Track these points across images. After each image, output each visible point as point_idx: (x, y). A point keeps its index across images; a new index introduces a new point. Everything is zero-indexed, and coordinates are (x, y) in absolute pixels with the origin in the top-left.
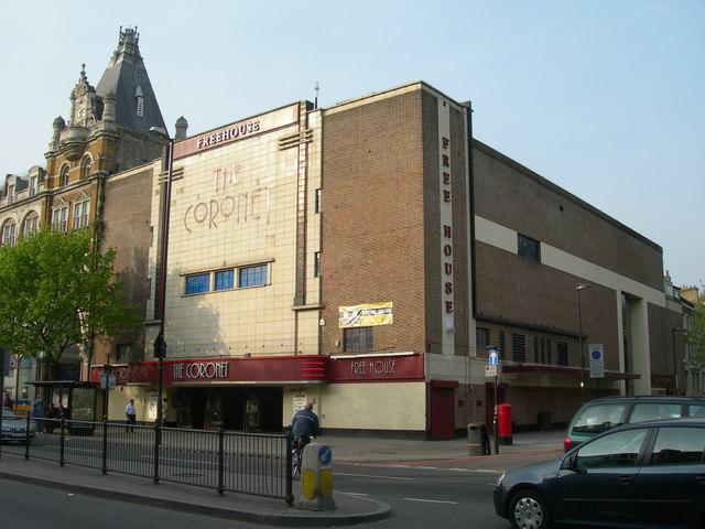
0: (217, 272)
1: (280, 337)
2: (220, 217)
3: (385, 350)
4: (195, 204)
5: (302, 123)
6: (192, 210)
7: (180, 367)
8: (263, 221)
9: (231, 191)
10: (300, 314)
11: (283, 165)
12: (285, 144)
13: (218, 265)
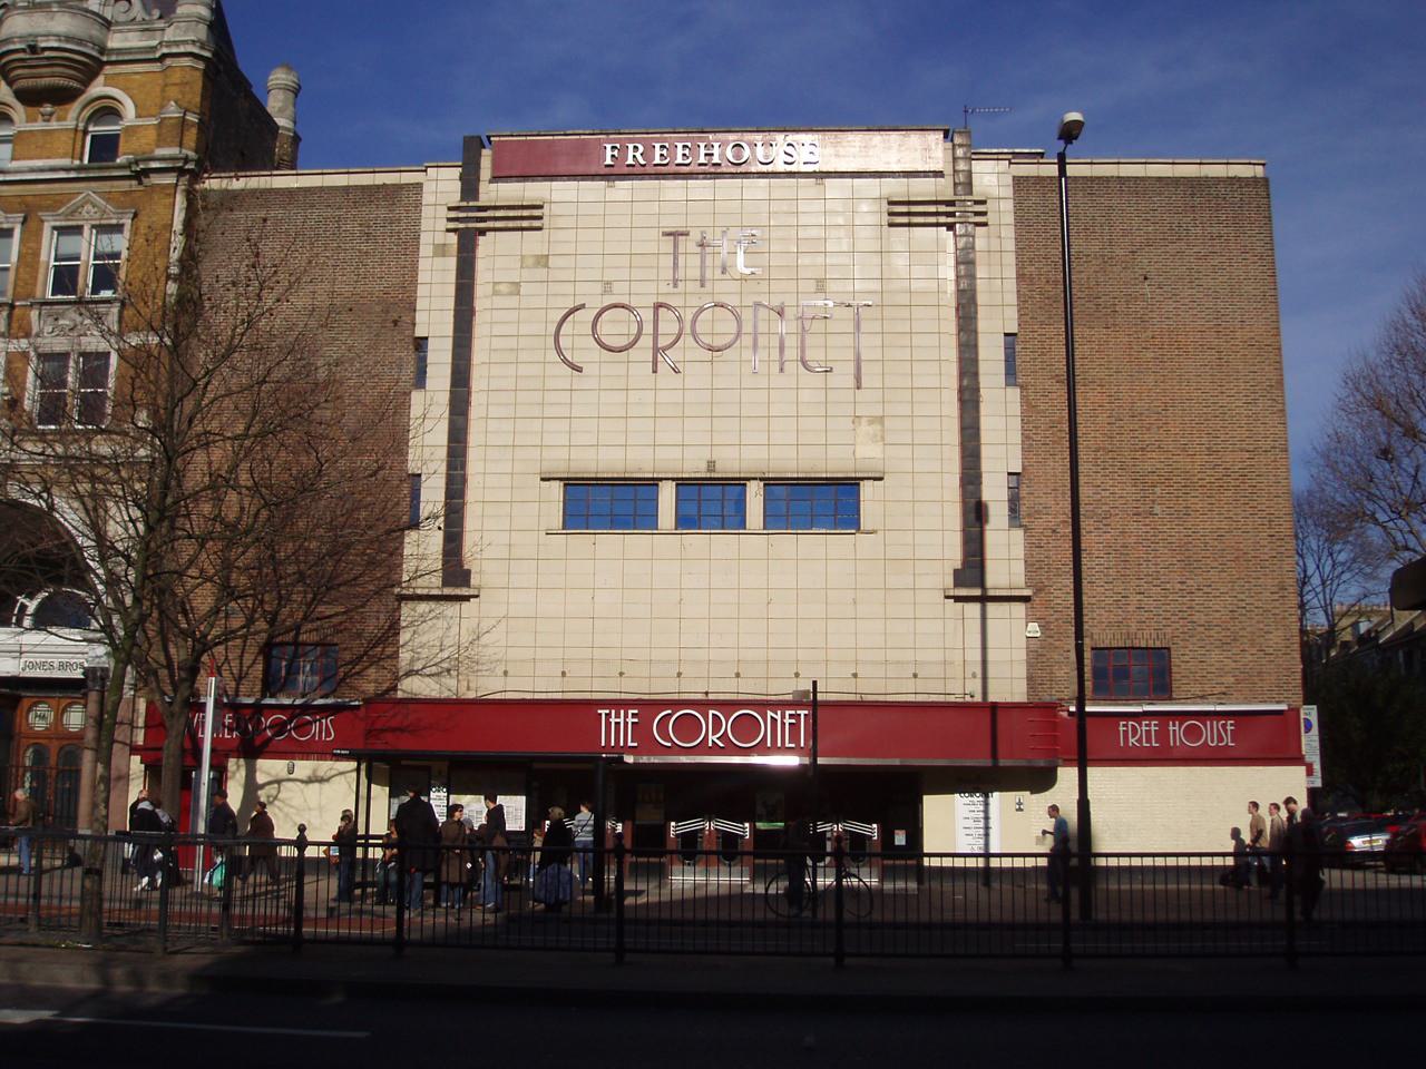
0: (682, 483)
1: (909, 655)
2: (687, 351)
3: (1203, 698)
4: (596, 303)
5: (950, 220)
6: (586, 316)
7: (1310, 588)
8: (843, 376)
9: (726, 291)
11: (900, 262)
12: (903, 213)
13: (695, 466)
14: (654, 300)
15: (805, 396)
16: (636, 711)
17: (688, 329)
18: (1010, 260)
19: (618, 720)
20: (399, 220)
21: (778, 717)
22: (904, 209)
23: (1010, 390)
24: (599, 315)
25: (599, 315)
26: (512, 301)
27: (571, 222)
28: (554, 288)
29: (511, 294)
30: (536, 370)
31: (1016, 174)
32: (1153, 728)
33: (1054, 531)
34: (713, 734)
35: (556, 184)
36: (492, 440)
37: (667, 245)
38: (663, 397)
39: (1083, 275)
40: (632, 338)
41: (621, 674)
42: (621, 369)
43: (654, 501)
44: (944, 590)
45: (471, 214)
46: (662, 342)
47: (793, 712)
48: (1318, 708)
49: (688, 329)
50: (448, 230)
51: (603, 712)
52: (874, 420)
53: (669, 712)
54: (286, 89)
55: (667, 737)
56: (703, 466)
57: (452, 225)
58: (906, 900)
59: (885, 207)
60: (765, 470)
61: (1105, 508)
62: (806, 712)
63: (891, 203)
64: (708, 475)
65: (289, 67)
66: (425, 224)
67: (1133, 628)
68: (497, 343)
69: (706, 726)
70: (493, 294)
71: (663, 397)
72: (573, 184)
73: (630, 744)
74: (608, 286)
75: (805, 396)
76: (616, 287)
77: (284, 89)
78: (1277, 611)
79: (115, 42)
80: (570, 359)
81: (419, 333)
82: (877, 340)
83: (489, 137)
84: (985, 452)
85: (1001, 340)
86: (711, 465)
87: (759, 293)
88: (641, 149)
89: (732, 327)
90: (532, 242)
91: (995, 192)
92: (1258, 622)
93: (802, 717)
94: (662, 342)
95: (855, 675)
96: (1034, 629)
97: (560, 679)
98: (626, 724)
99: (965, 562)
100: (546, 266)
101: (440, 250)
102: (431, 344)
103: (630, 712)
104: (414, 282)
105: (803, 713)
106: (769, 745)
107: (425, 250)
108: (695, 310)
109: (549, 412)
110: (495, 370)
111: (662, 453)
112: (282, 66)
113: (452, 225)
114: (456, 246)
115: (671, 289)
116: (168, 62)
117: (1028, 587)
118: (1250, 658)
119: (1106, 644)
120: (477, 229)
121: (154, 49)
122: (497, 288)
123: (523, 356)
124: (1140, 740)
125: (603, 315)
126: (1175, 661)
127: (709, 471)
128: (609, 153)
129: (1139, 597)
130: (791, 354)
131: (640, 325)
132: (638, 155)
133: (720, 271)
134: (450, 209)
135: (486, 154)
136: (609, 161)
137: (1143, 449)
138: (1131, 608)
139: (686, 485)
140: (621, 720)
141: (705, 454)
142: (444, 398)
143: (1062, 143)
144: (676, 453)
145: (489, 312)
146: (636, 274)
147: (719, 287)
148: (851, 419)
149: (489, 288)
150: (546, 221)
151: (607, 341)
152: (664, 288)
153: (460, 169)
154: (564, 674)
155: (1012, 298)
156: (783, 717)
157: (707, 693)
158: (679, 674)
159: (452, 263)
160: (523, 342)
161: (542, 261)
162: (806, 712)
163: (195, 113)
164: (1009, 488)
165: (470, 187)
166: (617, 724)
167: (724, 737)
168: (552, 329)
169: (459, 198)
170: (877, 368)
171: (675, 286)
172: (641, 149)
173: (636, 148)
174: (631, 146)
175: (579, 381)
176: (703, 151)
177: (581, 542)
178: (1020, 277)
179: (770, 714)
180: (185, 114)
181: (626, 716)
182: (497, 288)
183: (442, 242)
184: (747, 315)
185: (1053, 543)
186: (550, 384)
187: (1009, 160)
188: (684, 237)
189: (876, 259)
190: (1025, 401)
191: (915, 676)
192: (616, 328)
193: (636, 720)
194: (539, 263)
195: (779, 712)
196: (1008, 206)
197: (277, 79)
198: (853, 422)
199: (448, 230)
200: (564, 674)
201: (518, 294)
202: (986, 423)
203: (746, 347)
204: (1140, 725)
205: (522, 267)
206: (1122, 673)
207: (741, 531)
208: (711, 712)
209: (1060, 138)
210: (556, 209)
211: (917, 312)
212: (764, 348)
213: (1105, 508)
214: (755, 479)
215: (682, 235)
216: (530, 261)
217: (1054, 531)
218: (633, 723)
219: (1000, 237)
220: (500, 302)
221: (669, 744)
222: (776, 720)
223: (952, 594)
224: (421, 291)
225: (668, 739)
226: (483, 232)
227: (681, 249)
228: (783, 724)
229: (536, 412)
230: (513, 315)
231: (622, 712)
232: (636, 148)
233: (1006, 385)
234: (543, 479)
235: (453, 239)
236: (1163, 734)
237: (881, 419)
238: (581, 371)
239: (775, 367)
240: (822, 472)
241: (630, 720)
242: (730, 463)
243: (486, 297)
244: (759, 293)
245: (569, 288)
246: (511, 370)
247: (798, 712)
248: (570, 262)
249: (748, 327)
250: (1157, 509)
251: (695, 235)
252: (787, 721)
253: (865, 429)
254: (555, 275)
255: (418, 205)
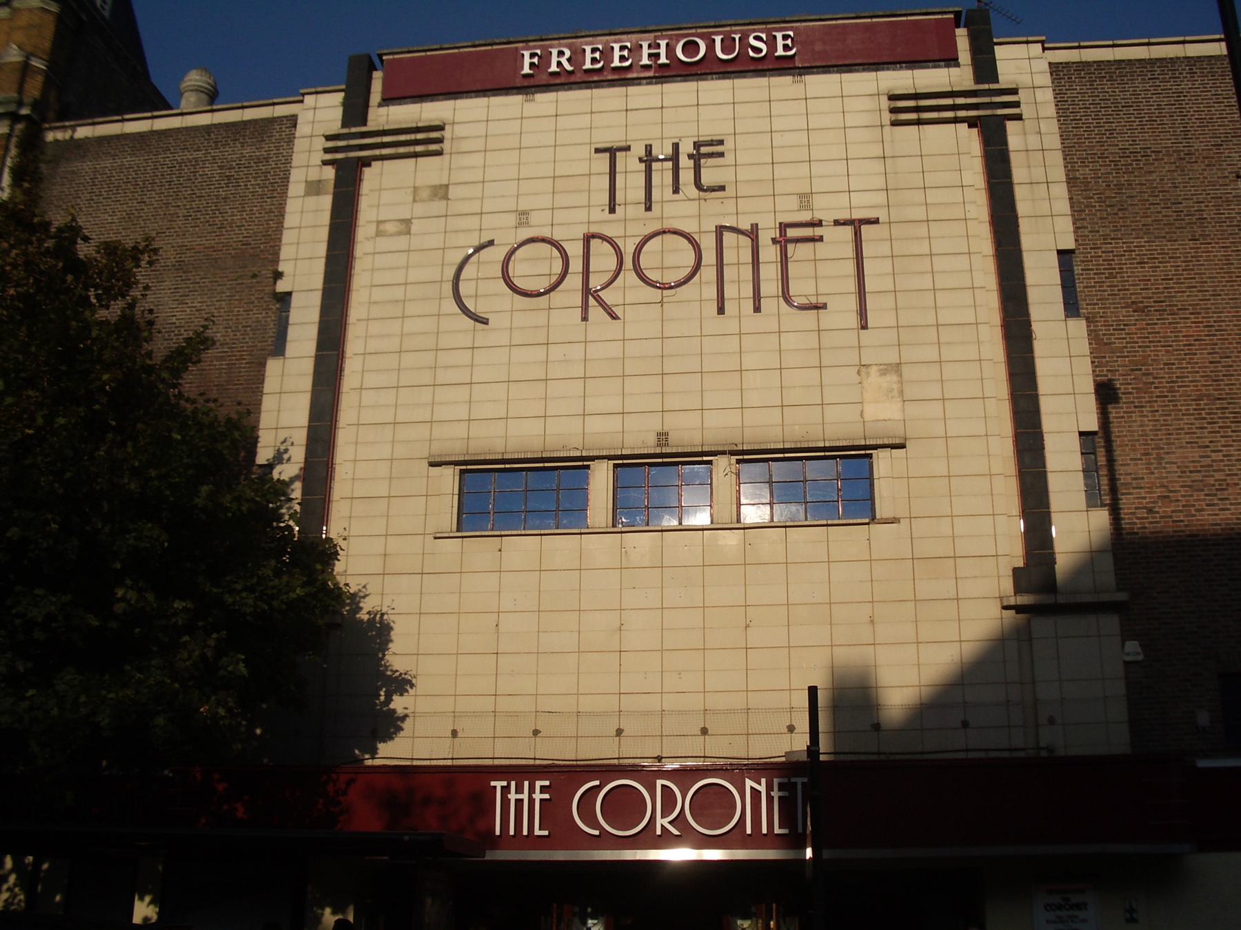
4: (513, 238)
8: (843, 311)
14: (580, 232)
15: (789, 341)
16: (547, 783)
18: (1056, 160)
19: (519, 796)
20: (267, 159)
21: (762, 788)
23: (1072, 323)
28: (455, 223)
29: (399, 233)
31: (1052, 61)
33: (1150, 511)
36: (367, 416)
38: (594, 351)
39: (1154, 176)
40: (554, 279)
41: (536, 733)
42: (541, 318)
43: (582, 490)
44: (1001, 598)
48: (132, 920)
50: (325, 163)
51: (499, 784)
53: (597, 783)
54: (198, 90)
55: (591, 821)
56: (652, 439)
57: (328, 157)
59: (885, 103)
60: (739, 440)
61: (1218, 476)
62: (805, 780)
63: (892, 98)
64: (658, 451)
65: (205, 69)
66: (297, 159)
68: (378, 294)
69: (653, 803)
70: (377, 236)
73: (537, 832)
74: (523, 217)
75: (789, 341)
76: (534, 218)
77: (196, 90)
81: (282, 286)
83: (380, 56)
84: (1046, 405)
85: (1054, 259)
86: (663, 437)
88: (568, 53)
89: (689, 258)
90: (428, 171)
93: (799, 787)
96: (1133, 648)
97: (449, 741)
98: (532, 801)
100: (446, 197)
101: (314, 188)
102: (296, 301)
103: (538, 784)
104: (280, 227)
107: (296, 187)
109: (442, 377)
110: (375, 328)
112: (195, 68)
113: (328, 157)
114: (333, 182)
115: (606, 215)
117: (1119, 590)
120: (359, 158)
122: (382, 227)
123: (411, 309)
128: (527, 61)
134: (329, 138)
135: (378, 76)
140: (525, 796)
141: (653, 424)
142: (306, 366)
144: (614, 424)
145: (370, 258)
146: (561, 200)
149: (372, 229)
150: (446, 146)
151: (519, 283)
153: (342, 94)
154: (454, 733)
155: (1063, 206)
157: (659, 759)
158: (619, 732)
159: (327, 201)
161: (441, 192)
162: (805, 780)
163: (42, 59)
164: (1082, 454)
165: (355, 111)
166: (519, 802)
167: (679, 821)
168: (450, 273)
169: (340, 126)
170: (889, 301)
173: (561, 53)
174: (555, 52)
175: (483, 336)
176: (646, 51)
177: (480, 550)
178: (1071, 181)
179: (749, 783)
180: (28, 58)
182: (382, 227)
183: (317, 178)
187: (1042, 42)
188: (624, 153)
189: (878, 167)
190: (1095, 339)
193: (547, 796)
194: (435, 195)
195: (763, 781)
196: (1046, 96)
197: (190, 80)
198: (859, 373)
199: (325, 163)
200: (454, 733)
202: (1043, 367)
205: (414, 201)
208: (659, 782)
210: (460, 131)
211: (935, 229)
213: (1218, 476)
214: (723, 453)
216: (425, 194)
217: (1150, 511)
218: (541, 800)
220: (384, 244)
221: (596, 833)
224: (288, 237)
225: (596, 825)
226: (367, 162)
227: (620, 167)
229: (426, 378)
230: (401, 259)
231: (526, 784)
232: (561, 53)
233: (1067, 316)
234: (432, 464)
235: (330, 173)
237: (897, 368)
238: (486, 323)
239: (749, 305)
241: (538, 796)
243: (368, 239)
244: (724, 215)
245: (473, 222)
247: (793, 780)
248: (476, 191)
249: (709, 257)
253: (874, 379)
254: (456, 207)
255: (290, 140)
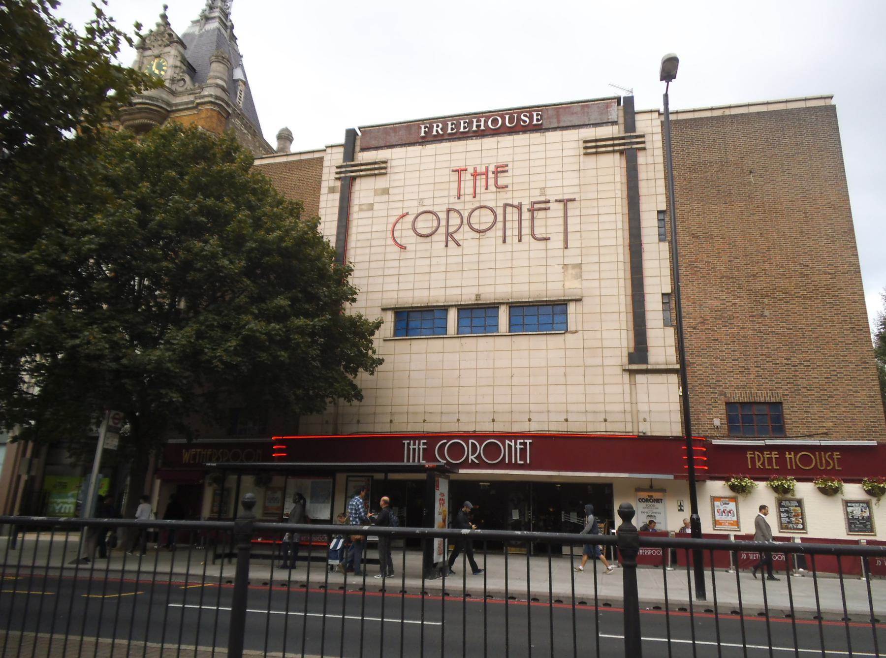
1: (601, 407)
4: (414, 211)
8: (557, 241)
10: (640, 378)
13: (468, 297)
14: (445, 208)
16: (425, 441)
17: (465, 221)
19: (414, 447)
21: (513, 444)
22: (593, 144)
23: (662, 244)
24: (417, 217)
25: (417, 217)
26: (369, 214)
27: (402, 169)
28: (392, 205)
30: (382, 249)
32: (422, 447)
34: (472, 455)
35: (395, 150)
37: (455, 177)
40: (434, 229)
42: (428, 246)
45: (348, 169)
46: (451, 230)
47: (522, 441)
49: (465, 221)
51: (406, 442)
52: (575, 266)
53: (445, 441)
56: (474, 297)
58: (87, 604)
61: (729, 313)
62: (531, 441)
63: (585, 142)
64: (476, 302)
66: (324, 177)
67: (755, 389)
68: (360, 237)
71: (450, 260)
72: (403, 149)
75: (533, 254)
76: (426, 202)
78: (862, 378)
79: (178, 100)
80: (400, 243)
82: (578, 220)
84: (647, 282)
87: (507, 199)
88: (441, 126)
90: (381, 183)
91: (649, 130)
92: (848, 385)
94: (451, 230)
95: (566, 420)
98: (419, 449)
99: (636, 348)
101: (332, 190)
103: (422, 441)
105: (528, 441)
106: (750, 467)
107: (324, 190)
108: (469, 211)
111: (449, 292)
113: (338, 176)
115: (456, 200)
116: (200, 107)
118: (844, 409)
119: (736, 400)
121: (192, 102)
124: (763, 464)
125: (419, 218)
126: (786, 412)
127: (477, 300)
128: (423, 130)
129: (757, 369)
130: (526, 231)
131: (439, 219)
132: (439, 129)
133: (484, 188)
136: (423, 134)
137: (754, 276)
138: (752, 376)
139: (463, 309)
140: (416, 447)
141: (475, 291)
143: (664, 83)
144: (458, 291)
146: (437, 194)
147: (484, 197)
148: (561, 266)
150: (388, 170)
152: (452, 200)
156: (516, 444)
160: (374, 235)
161: (386, 191)
162: (531, 441)
164: (663, 303)
166: (414, 449)
168: (390, 227)
171: (459, 198)
172: (441, 126)
173: (438, 126)
174: (435, 125)
176: (475, 124)
179: (507, 442)
181: (419, 444)
184: (500, 212)
185: (694, 336)
186: (388, 257)
189: (576, 174)
191: (605, 420)
192: (425, 225)
193: (425, 447)
195: (513, 441)
201: (373, 209)
203: (499, 229)
204: (763, 454)
206: (748, 419)
207: (495, 334)
208: (470, 441)
209: (661, 80)
210: (394, 163)
212: (510, 228)
213: (729, 313)
215: (463, 170)
217: (694, 328)
218: (423, 448)
219: (653, 155)
220: (363, 214)
222: (511, 446)
223: (627, 368)
228: (516, 449)
229: (380, 272)
230: (370, 221)
231: (417, 442)
232: (438, 126)
236: (781, 461)
240: (543, 297)
241: (422, 447)
242: (489, 294)
244: (507, 199)
245: (400, 205)
246: (367, 251)
247: (525, 441)
250: (767, 313)
251: (471, 170)
252: (518, 446)
254: (392, 198)
